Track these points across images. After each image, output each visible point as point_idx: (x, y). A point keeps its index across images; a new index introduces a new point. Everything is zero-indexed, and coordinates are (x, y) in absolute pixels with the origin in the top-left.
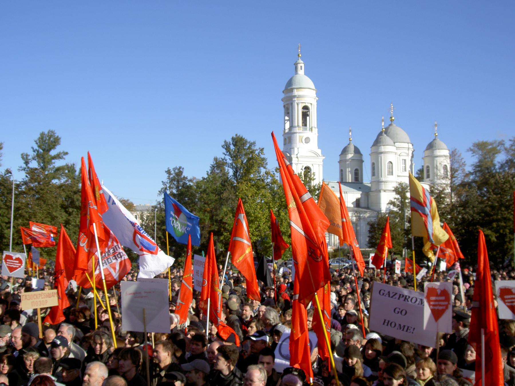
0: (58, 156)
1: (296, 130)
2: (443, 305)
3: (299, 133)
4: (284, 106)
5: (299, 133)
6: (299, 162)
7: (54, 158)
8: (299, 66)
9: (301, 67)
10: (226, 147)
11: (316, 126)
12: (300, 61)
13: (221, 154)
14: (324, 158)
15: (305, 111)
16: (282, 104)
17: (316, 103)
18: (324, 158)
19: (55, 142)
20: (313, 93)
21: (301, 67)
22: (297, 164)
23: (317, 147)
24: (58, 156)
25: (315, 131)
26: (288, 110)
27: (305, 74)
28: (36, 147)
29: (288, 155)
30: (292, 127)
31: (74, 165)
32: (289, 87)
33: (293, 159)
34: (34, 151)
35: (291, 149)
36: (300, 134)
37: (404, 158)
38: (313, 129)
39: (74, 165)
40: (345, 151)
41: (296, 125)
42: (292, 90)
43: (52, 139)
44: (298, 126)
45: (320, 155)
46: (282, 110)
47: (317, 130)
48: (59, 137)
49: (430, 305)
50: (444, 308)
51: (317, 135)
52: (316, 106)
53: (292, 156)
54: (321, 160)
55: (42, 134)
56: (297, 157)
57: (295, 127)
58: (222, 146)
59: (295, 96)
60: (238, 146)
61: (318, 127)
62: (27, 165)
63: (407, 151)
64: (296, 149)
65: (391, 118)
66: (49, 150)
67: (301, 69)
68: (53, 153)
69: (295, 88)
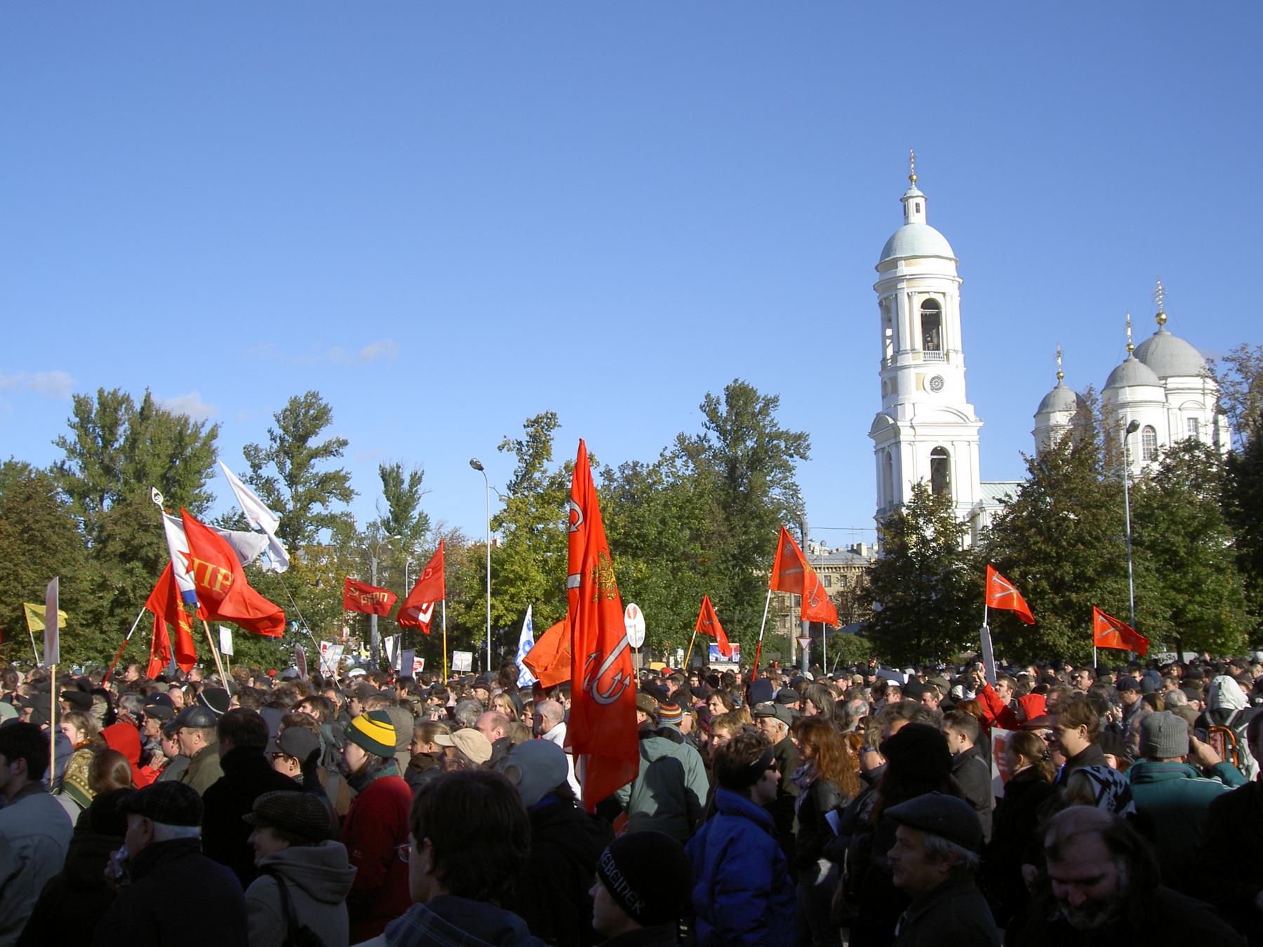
0: (326, 451)
1: (907, 360)
3: (916, 366)
4: (881, 304)
5: (916, 366)
6: (918, 438)
7: (315, 454)
8: (912, 203)
9: (917, 205)
10: (709, 407)
11: (959, 347)
12: (915, 191)
13: (696, 426)
14: (981, 424)
15: (928, 312)
16: (874, 298)
17: (957, 293)
18: (981, 424)
19: (316, 418)
20: (950, 268)
21: (917, 205)
22: (911, 443)
23: (964, 400)
24: (326, 451)
25: (958, 359)
26: (889, 313)
27: (928, 222)
28: (279, 431)
29: (891, 421)
30: (897, 352)
31: (399, 467)
32: (888, 261)
33: (903, 431)
34: (274, 439)
35: (896, 406)
36: (918, 368)
37: (1193, 414)
38: (952, 355)
39: (399, 467)
40: (1045, 407)
41: (908, 347)
42: (894, 264)
43: (312, 412)
44: (913, 350)
45: (972, 417)
46: (877, 313)
47: (961, 356)
48: (730, 383)
49: (998, 764)
51: (962, 370)
52: (957, 299)
53: (899, 424)
54: (975, 431)
55: (294, 402)
56: (912, 427)
57: (906, 352)
58: (701, 407)
59: (901, 279)
60: (740, 409)
61: (963, 352)
62: (255, 472)
63: (1200, 398)
64: (908, 408)
65: (1158, 315)
66: (303, 439)
67: (918, 211)
68: (313, 443)
69: (901, 259)
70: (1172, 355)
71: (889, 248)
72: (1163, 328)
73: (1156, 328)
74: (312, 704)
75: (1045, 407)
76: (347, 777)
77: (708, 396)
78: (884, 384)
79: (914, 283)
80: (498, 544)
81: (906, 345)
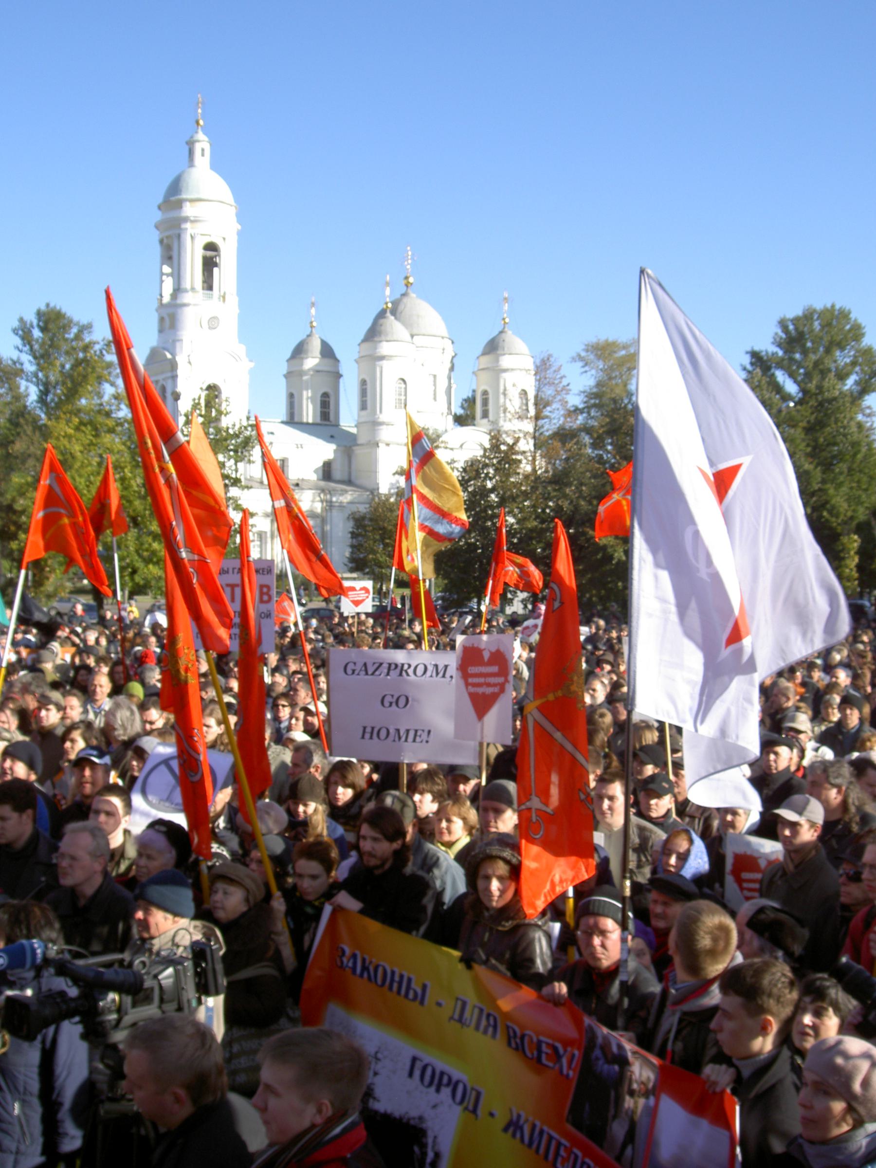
1: (186, 298)
2: (495, 685)
4: (161, 242)
8: (198, 147)
9: (203, 150)
12: (201, 136)
15: (210, 253)
16: (156, 236)
21: (203, 150)
25: (233, 300)
26: (170, 251)
29: (169, 356)
36: (197, 307)
40: (299, 351)
42: (179, 204)
44: (193, 289)
46: (156, 251)
50: (496, 690)
51: (237, 311)
53: (178, 359)
57: (186, 291)
59: (186, 219)
67: (203, 155)
70: (418, 316)
71: (175, 187)
72: (409, 291)
73: (403, 290)
74: (328, 854)
75: (299, 351)
76: (129, 881)
77: (21, 320)
78: (162, 320)
79: (198, 225)
80: (475, 600)
81: (187, 284)
